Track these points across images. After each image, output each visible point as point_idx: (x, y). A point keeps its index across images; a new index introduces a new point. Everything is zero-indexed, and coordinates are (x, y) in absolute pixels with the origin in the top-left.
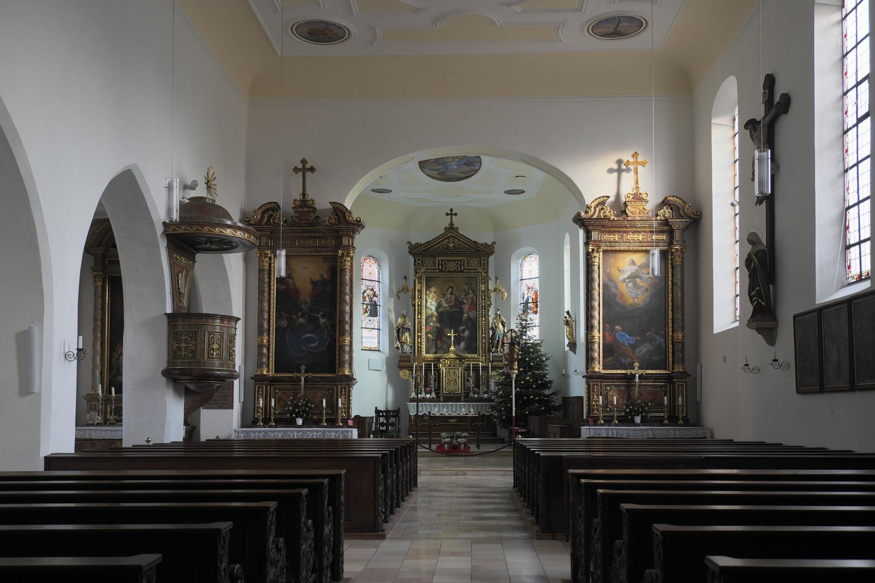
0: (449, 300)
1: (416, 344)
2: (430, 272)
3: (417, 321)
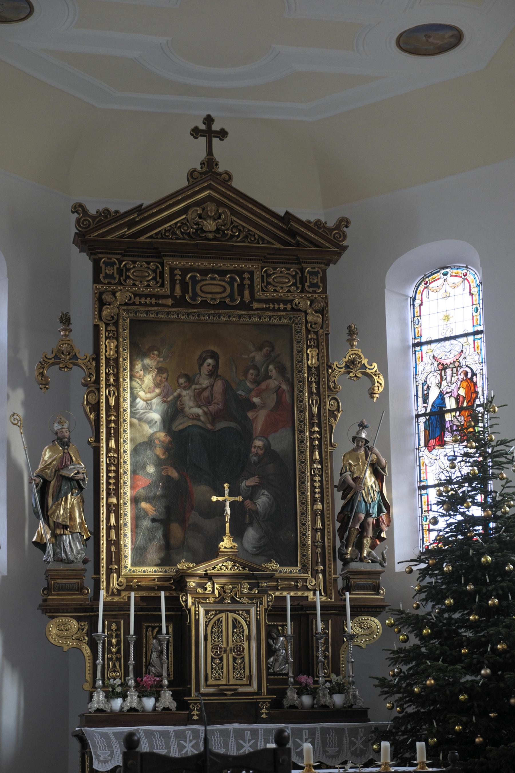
0: (206, 394)
1: (103, 533)
2: (145, 305)
3: (103, 459)
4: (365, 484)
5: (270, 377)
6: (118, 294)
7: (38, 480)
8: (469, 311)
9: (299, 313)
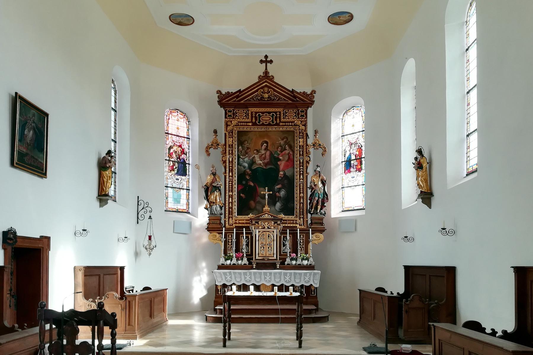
0: (263, 156)
2: (242, 125)
4: (318, 187)
5: (286, 150)
6: (233, 122)
7: (205, 187)
8: (361, 122)
9: (297, 126)
